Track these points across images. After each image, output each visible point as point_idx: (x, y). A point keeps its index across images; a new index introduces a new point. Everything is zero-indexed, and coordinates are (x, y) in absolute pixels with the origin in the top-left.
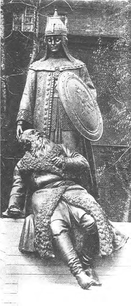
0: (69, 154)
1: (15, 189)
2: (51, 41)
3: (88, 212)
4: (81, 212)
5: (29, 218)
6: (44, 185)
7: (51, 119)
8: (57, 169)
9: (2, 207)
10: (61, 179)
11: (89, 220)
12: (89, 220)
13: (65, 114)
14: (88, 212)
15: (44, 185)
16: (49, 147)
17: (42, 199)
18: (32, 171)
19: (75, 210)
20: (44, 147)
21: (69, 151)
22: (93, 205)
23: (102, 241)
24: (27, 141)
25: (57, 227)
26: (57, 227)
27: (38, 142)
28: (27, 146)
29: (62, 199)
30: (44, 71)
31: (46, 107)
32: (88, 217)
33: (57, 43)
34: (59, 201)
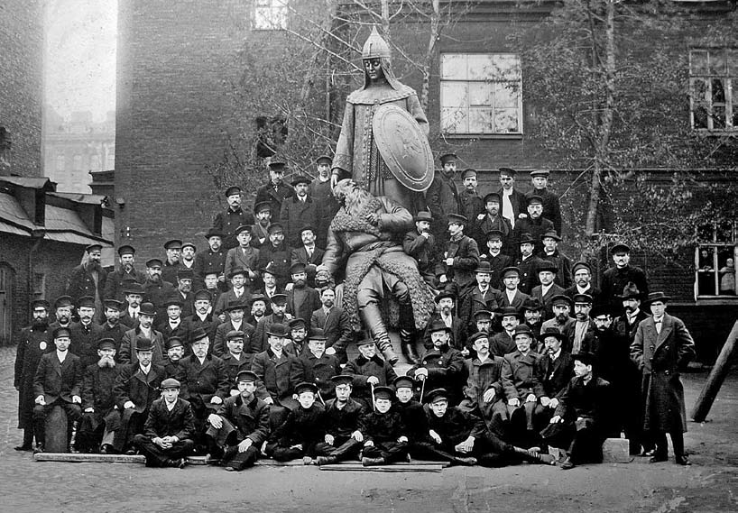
0: (390, 208)
1: (701, 65)
2: (369, 66)
3: (401, 280)
4: (394, 280)
5: (339, 288)
6: (357, 248)
7: (370, 165)
8: (373, 228)
9: (218, 412)
10: (379, 239)
11: (403, 288)
12: (403, 288)
13: (379, 158)
14: (401, 280)
15: (357, 248)
16: (365, 201)
17: (356, 265)
18: (344, 231)
19: (388, 276)
20: (359, 202)
21: (389, 205)
22: (406, 271)
23: (416, 313)
24: (342, 195)
25: (364, 295)
26: (364, 295)
27: (352, 195)
28: (340, 202)
29: (375, 264)
30: (360, 104)
31: (364, 150)
32: (401, 285)
33: (376, 68)
34: (372, 266)
